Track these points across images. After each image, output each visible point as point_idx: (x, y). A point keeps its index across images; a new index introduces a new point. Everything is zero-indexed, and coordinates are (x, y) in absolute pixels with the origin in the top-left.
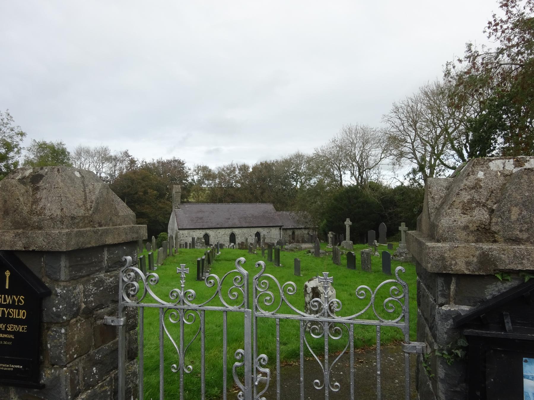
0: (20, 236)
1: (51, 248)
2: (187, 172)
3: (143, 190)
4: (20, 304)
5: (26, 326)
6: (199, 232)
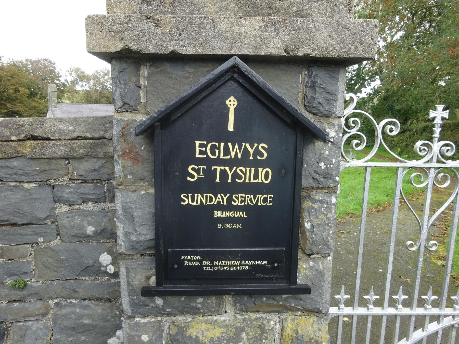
0: (278, 26)
1: (345, 52)
3: (13, 87)
4: (258, 157)
5: (272, 196)
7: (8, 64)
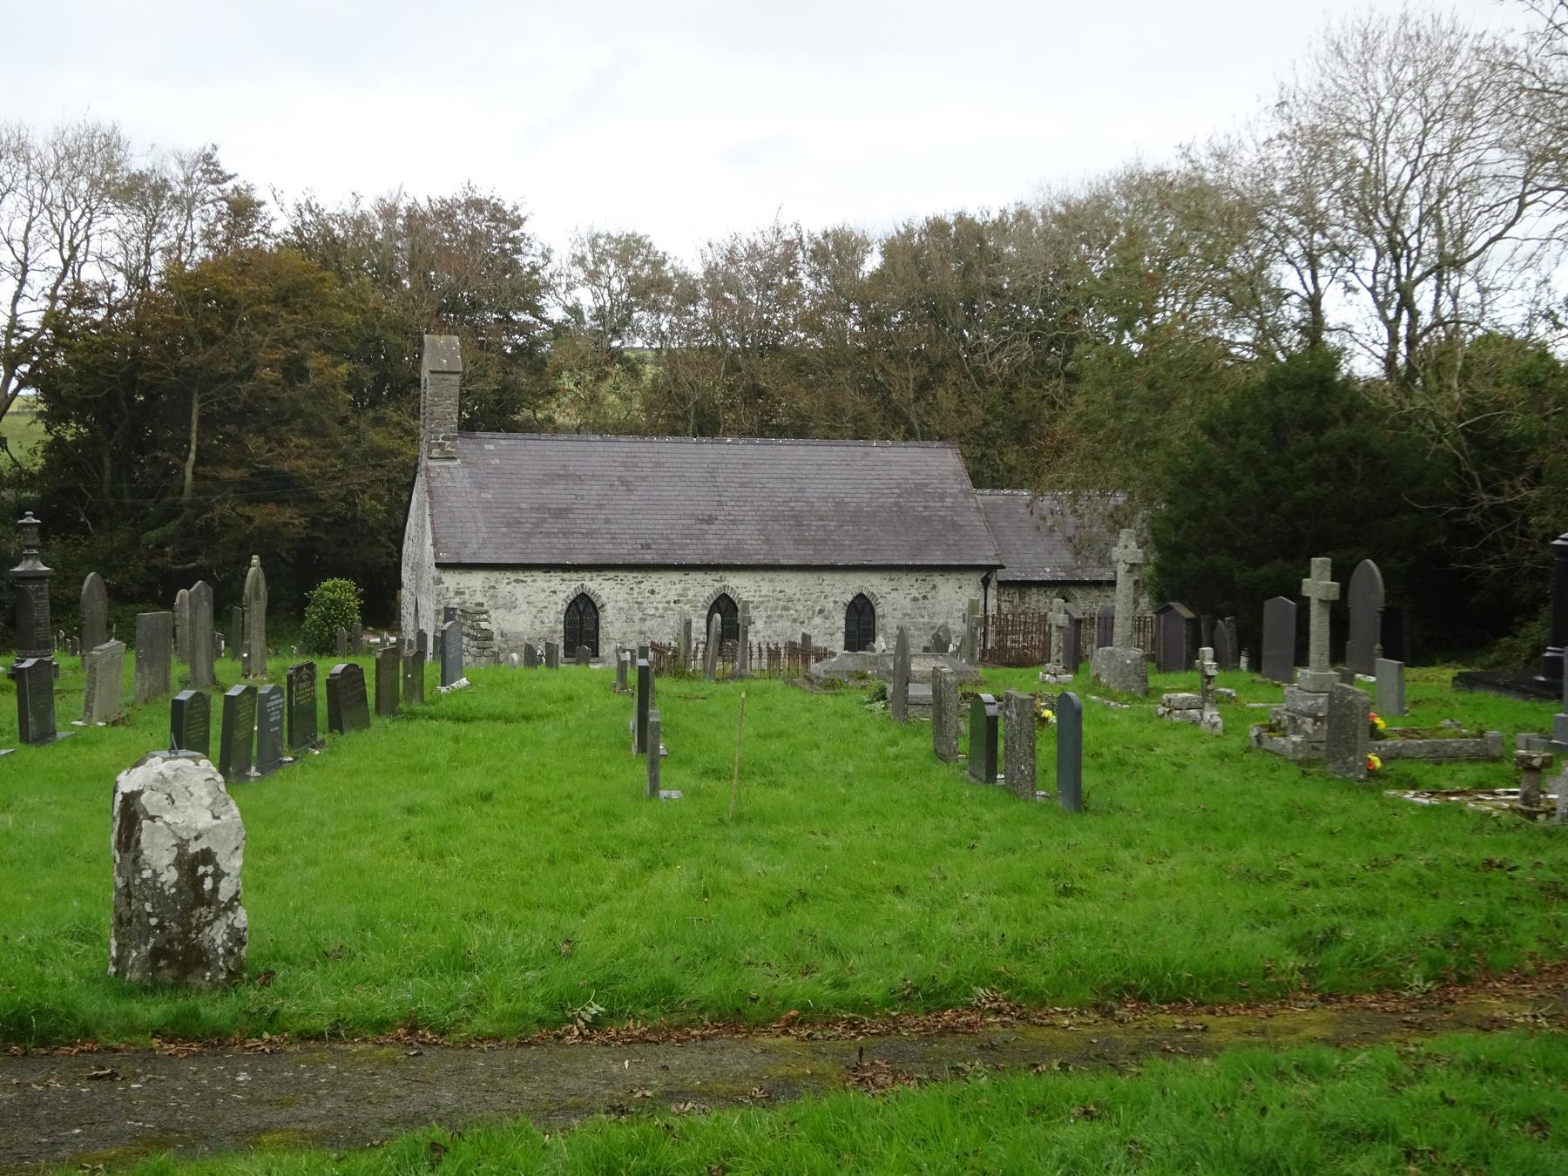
2: (535, 270)
3: (280, 354)
6: (545, 585)
7: (295, 238)
